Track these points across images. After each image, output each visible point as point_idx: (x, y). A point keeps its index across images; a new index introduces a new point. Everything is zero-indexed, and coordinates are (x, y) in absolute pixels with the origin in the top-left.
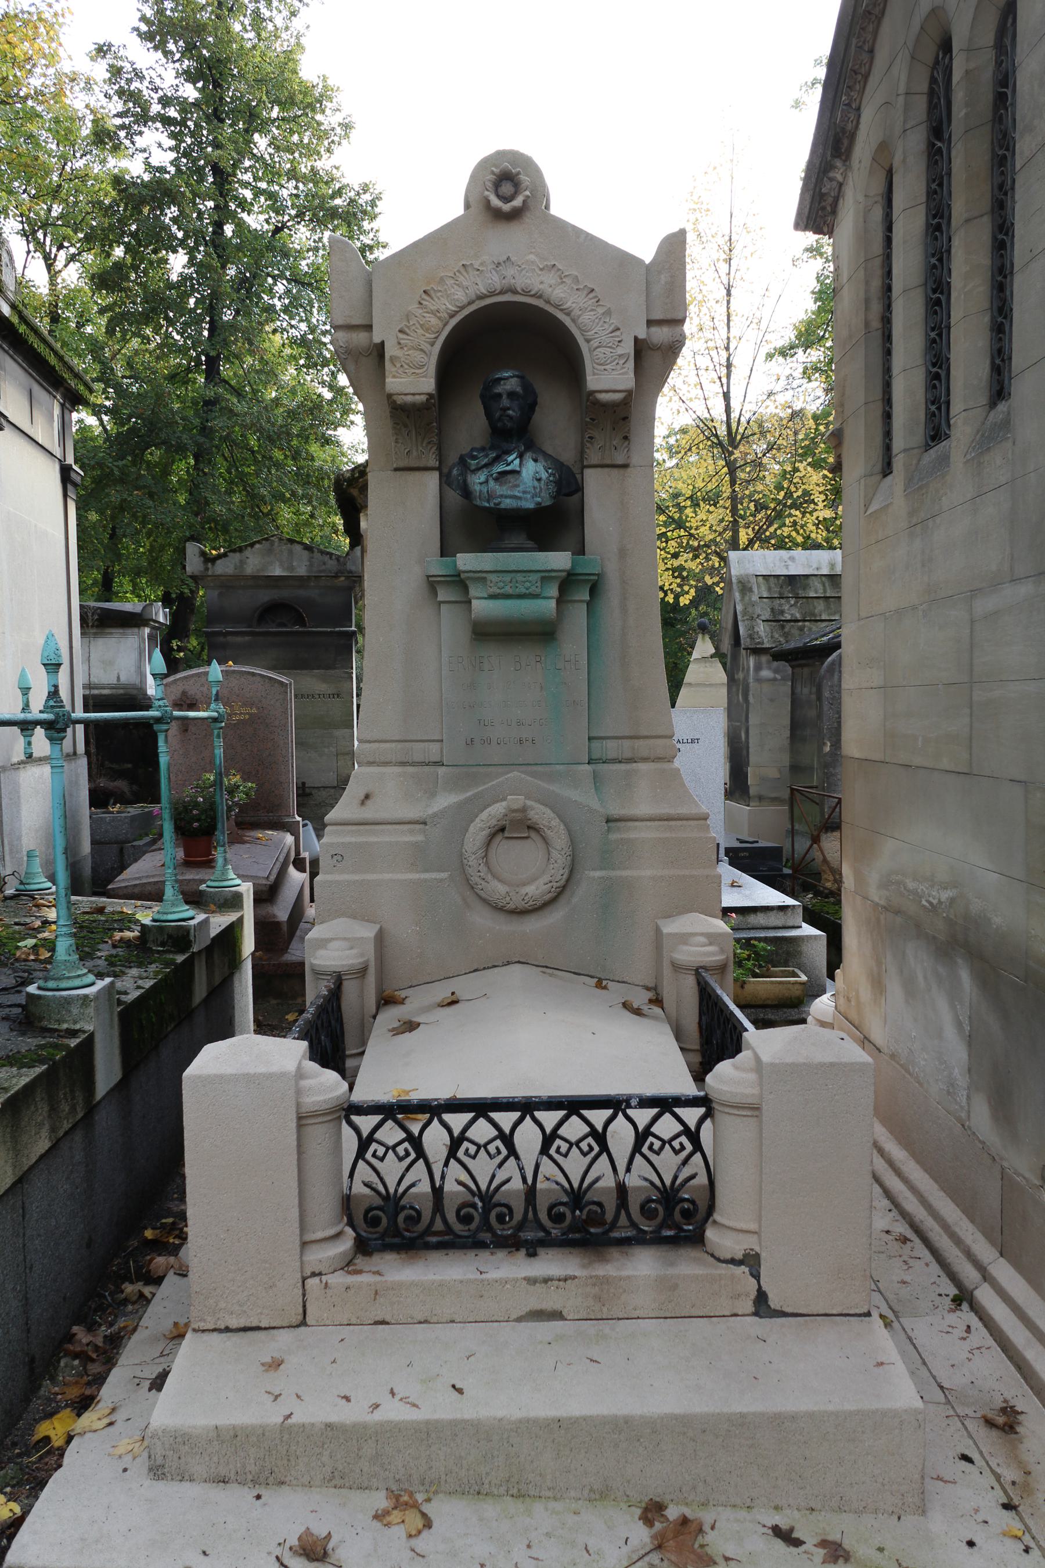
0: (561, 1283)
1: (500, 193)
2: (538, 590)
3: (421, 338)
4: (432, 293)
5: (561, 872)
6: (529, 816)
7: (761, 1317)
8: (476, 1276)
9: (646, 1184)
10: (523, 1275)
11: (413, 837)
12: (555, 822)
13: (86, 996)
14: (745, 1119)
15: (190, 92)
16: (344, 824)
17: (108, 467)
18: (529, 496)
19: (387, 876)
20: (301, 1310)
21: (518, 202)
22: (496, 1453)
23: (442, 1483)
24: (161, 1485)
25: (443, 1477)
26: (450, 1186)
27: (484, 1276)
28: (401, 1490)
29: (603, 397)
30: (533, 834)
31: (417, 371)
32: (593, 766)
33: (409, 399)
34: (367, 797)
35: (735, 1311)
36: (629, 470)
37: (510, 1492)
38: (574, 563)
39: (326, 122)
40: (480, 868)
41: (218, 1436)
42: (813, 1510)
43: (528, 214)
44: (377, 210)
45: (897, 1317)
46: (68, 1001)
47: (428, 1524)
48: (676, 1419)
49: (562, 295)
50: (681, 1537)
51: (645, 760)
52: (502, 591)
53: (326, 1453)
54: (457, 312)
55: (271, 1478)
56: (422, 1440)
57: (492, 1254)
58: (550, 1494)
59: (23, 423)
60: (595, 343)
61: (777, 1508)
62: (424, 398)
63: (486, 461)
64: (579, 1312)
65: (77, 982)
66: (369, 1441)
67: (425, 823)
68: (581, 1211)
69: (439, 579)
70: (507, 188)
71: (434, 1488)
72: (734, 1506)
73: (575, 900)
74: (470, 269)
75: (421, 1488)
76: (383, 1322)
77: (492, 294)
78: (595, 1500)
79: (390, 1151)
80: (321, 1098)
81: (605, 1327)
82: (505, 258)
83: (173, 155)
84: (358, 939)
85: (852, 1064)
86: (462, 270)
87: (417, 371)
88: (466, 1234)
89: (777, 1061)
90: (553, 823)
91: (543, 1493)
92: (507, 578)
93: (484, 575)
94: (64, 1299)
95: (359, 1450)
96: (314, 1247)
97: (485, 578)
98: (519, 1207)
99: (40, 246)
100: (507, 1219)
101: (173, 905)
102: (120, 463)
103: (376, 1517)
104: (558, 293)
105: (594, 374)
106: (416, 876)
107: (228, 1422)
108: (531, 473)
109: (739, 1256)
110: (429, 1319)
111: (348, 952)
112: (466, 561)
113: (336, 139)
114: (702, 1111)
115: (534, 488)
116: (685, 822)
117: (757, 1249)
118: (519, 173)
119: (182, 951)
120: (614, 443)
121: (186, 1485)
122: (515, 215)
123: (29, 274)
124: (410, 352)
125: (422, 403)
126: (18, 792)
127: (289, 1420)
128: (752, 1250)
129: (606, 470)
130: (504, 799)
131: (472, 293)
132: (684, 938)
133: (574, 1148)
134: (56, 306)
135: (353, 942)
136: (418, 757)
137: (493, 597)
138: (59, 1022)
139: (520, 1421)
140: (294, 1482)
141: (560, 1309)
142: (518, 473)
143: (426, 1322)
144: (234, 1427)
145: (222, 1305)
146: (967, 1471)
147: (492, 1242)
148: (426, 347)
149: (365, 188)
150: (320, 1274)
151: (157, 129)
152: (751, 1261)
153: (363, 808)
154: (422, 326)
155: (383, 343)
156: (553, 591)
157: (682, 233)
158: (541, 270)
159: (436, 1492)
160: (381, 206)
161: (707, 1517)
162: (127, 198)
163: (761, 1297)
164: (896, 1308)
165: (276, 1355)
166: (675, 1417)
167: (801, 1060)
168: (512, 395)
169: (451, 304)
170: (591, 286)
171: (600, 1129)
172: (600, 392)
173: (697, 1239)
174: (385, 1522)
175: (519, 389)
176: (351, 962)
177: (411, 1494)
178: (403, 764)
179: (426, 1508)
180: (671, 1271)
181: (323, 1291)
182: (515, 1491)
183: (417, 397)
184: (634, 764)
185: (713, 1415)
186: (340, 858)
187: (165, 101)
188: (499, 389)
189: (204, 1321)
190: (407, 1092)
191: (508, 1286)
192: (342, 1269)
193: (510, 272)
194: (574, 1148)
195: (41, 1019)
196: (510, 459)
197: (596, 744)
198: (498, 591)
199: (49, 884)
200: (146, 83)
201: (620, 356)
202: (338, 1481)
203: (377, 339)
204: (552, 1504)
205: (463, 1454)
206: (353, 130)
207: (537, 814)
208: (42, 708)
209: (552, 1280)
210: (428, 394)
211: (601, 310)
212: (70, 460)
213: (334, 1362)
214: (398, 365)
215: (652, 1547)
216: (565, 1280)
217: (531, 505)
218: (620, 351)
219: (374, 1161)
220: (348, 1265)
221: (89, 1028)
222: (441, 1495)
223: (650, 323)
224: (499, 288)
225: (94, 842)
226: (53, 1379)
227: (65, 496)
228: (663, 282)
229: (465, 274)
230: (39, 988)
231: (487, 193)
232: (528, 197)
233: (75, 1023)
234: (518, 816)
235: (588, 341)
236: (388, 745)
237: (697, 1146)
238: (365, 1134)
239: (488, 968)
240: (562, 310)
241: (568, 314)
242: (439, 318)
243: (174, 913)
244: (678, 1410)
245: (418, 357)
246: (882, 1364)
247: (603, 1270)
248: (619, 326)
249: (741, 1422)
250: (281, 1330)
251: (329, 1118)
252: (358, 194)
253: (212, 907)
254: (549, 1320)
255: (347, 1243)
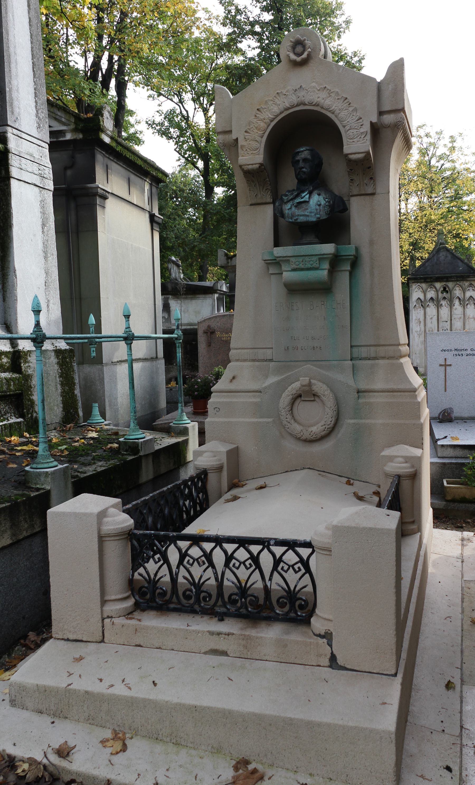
0: (226, 636)
1: (296, 52)
2: (318, 265)
3: (256, 134)
4: (261, 110)
5: (331, 420)
6: (313, 389)
7: (333, 669)
8: (184, 627)
9: (280, 588)
10: (207, 630)
11: (255, 399)
12: (328, 392)
13: (47, 472)
14: (327, 556)
15: (267, 17)
16: (221, 392)
17: (222, 214)
18: (313, 214)
19: (241, 420)
20: (101, 634)
21: (305, 56)
22: (165, 719)
23: (140, 730)
24: (13, 709)
25: (140, 727)
26: (181, 580)
27: (188, 628)
28: (120, 731)
29: (353, 157)
30: (317, 399)
31: (254, 152)
32: (354, 362)
33: (250, 167)
34: (234, 378)
35: (319, 664)
36: (375, 196)
37: (172, 741)
38: (337, 250)
39: (337, 22)
40: (287, 417)
41: (38, 689)
42: (331, 779)
43: (312, 61)
44: (363, 65)
45: (462, 684)
46: (39, 474)
47: (124, 748)
48: (256, 716)
49: (329, 103)
50: (247, 780)
51: (383, 358)
52: (298, 267)
53: (86, 706)
54: (274, 118)
55: (61, 715)
56: (130, 707)
57: (202, 617)
58: (191, 745)
59: (123, 193)
60: (348, 128)
61: (311, 775)
62: (257, 166)
63: (292, 197)
64: (235, 653)
65: (46, 465)
66: (105, 703)
67: (260, 392)
68: (245, 599)
69: (269, 262)
70: (299, 49)
71: (136, 733)
72: (288, 769)
73: (340, 435)
74: (281, 95)
75: (130, 732)
76: (140, 646)
77: (293, 107)
78: (214, 753)
79: (291, 568)
80: (112, 527)
81: (247, 662)
82: (299, 86)
83: (258, 51)
84: (219, 452)
85: (382, 529)
86: (277, 96)
87: (254, 152)
88: (187, 605)
89: (339, 525)
90: (326, 393)
91: (188, 745)
92: (301, 259)
93: (288, 258)
94: (24, 618)
95: (100, 707)
96: (111, 603)
97: (289, 260)
98: (214, 593)
99: (201, 105)
100: (208, 599)
101: (133, 431)
102: (228, 211)
103: (102, 742)
104: (328, 102)
105: (348, 145)
106: (256, 420)
107: (42, 683)
108: (315, 202)
109: (323, 633)
110: (161, 647)
111: (211, 458)
112: (279, 252)
113: (342, 30)
114: (310, 550)
115: (316, 209)
116: (402, 393)
117: (332, 630)
118: (305, 40)
119: (134, 455)
120: (365, 182)
121: (25, 711)
122: (304, 63)
123: (196, 120)
124: (250, 142)
125: (257, 169)
126: (116, 376)
127: (69, 687)
128: (329, 630)
129: (362, 197)
130: (299, 380)
131: (282, 107)
132: (391, 458)
133: (196, 563)
134: (209, 134)
135: (215, 454)
136: (261, 357)
137: (294, 270)
138: (36, 484)
139: (176, 704)
140: (72, 718)
141: (226, 650)
142: (308, 202)
143: (160, 648)
144: (45, 686)
145: (66, 627)
146: (443, 775)
147: (200, 611)
148: (258, 139)
149: (355, 54)
150: (112, 617)
151: (250, 39)
152: (328, 636)
153: (231, 384)
154: (256, 128)
155: (237, 139)
156: (326, 265)
157: (401, 61)
158: (319, 90)
159: (136, 735)
160: (364, 63)
161: (269, 773)
162: (232, 75)
163: (333, 658)
164: (465, 678)
165: (82, 655)
166: (255, 715)
167: (353, 525)
168: (305, 160)
169: (271, 114)
170: (345, 96)
171: (305, 558)
172: (351, 154)
173: (306, 622)
174: (104, 745)
175: (309, 157)
176: (212, 463)
177: (124, 734)
178: (254, 360)
179: (128, 742)
180: (286, 637)
181: (112, 626)
182: (174, 741)
183: (254, 166)
184: (377, 361)
185: (275, 717)
186: (218, 410)
187: (252, 24)
188: (298, 158)
189: (58, 634)
190: (204, 531)
191: (200, 635)
192: (124, 616)
193: (301, 94)
194: (196, 563)
195: (28, 483)
196: (303, 195)
197: (355, 350)
198: (296, 267)
199: (103, 420)
200: (243, 16)
201: (362, 133)
202: (90, 721)
203: (234, 138)
204: (193, 752)
205: (149, 717)
206: (351, 24)
207: (317, 387)
208: (32, 332)
209: (221, 634)
210: (259, 164)
211: (351, 109)
212: (156, 212)
213: (107, 662)
214: (245, 150)
215: (231, 782)
216: (228, 635)
217: (314, 219)
218: (362, 130)
219: (188, 566)
220: (128, 614)
221: (48, 488)
222: (139, 737)
223: (381, 113)
224: (296, 103)
225: (167, 403)
226: (9, 655)
227: (152, 229)
228: (390, 89)
229: (278, 97)
230: (31, 468)
231: (288, 53)
232: (309, 52)
233: (42, 485)
234: (307, 388)
235: (344, 127)
236: (246, 351)
237: (308, 570)
238: (278, 557)
239: (293, 471)
240: (330, 111)
241: (333, 113)
242: (265, 123)
243: (133, 435)
244: (257, 711)
245: (255, 144)
246: (385, 703)
247: (253, 632)
248: (361, 117)
249: (290, 722)
250: (92, 643)
251: (118, 538)
252: (351, 58)
253: (173, 434)
254: (220, 656)
255: (131, 602)
